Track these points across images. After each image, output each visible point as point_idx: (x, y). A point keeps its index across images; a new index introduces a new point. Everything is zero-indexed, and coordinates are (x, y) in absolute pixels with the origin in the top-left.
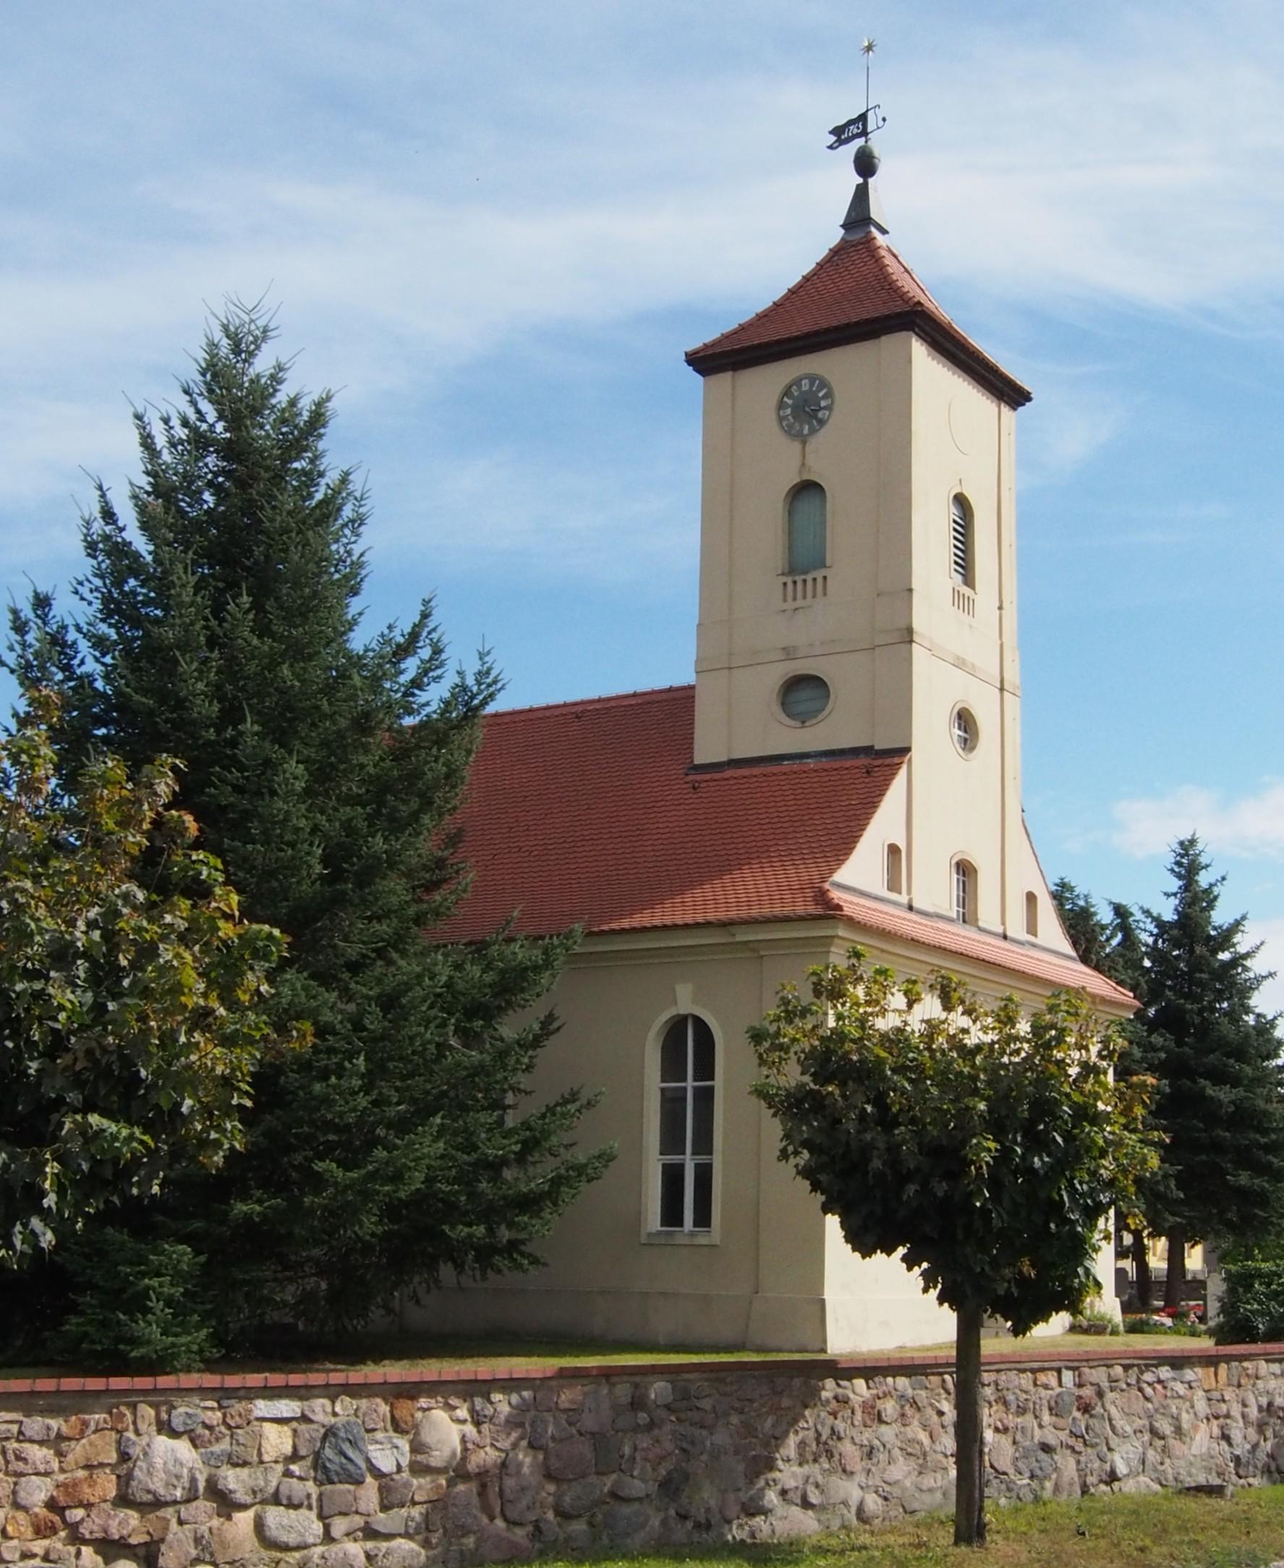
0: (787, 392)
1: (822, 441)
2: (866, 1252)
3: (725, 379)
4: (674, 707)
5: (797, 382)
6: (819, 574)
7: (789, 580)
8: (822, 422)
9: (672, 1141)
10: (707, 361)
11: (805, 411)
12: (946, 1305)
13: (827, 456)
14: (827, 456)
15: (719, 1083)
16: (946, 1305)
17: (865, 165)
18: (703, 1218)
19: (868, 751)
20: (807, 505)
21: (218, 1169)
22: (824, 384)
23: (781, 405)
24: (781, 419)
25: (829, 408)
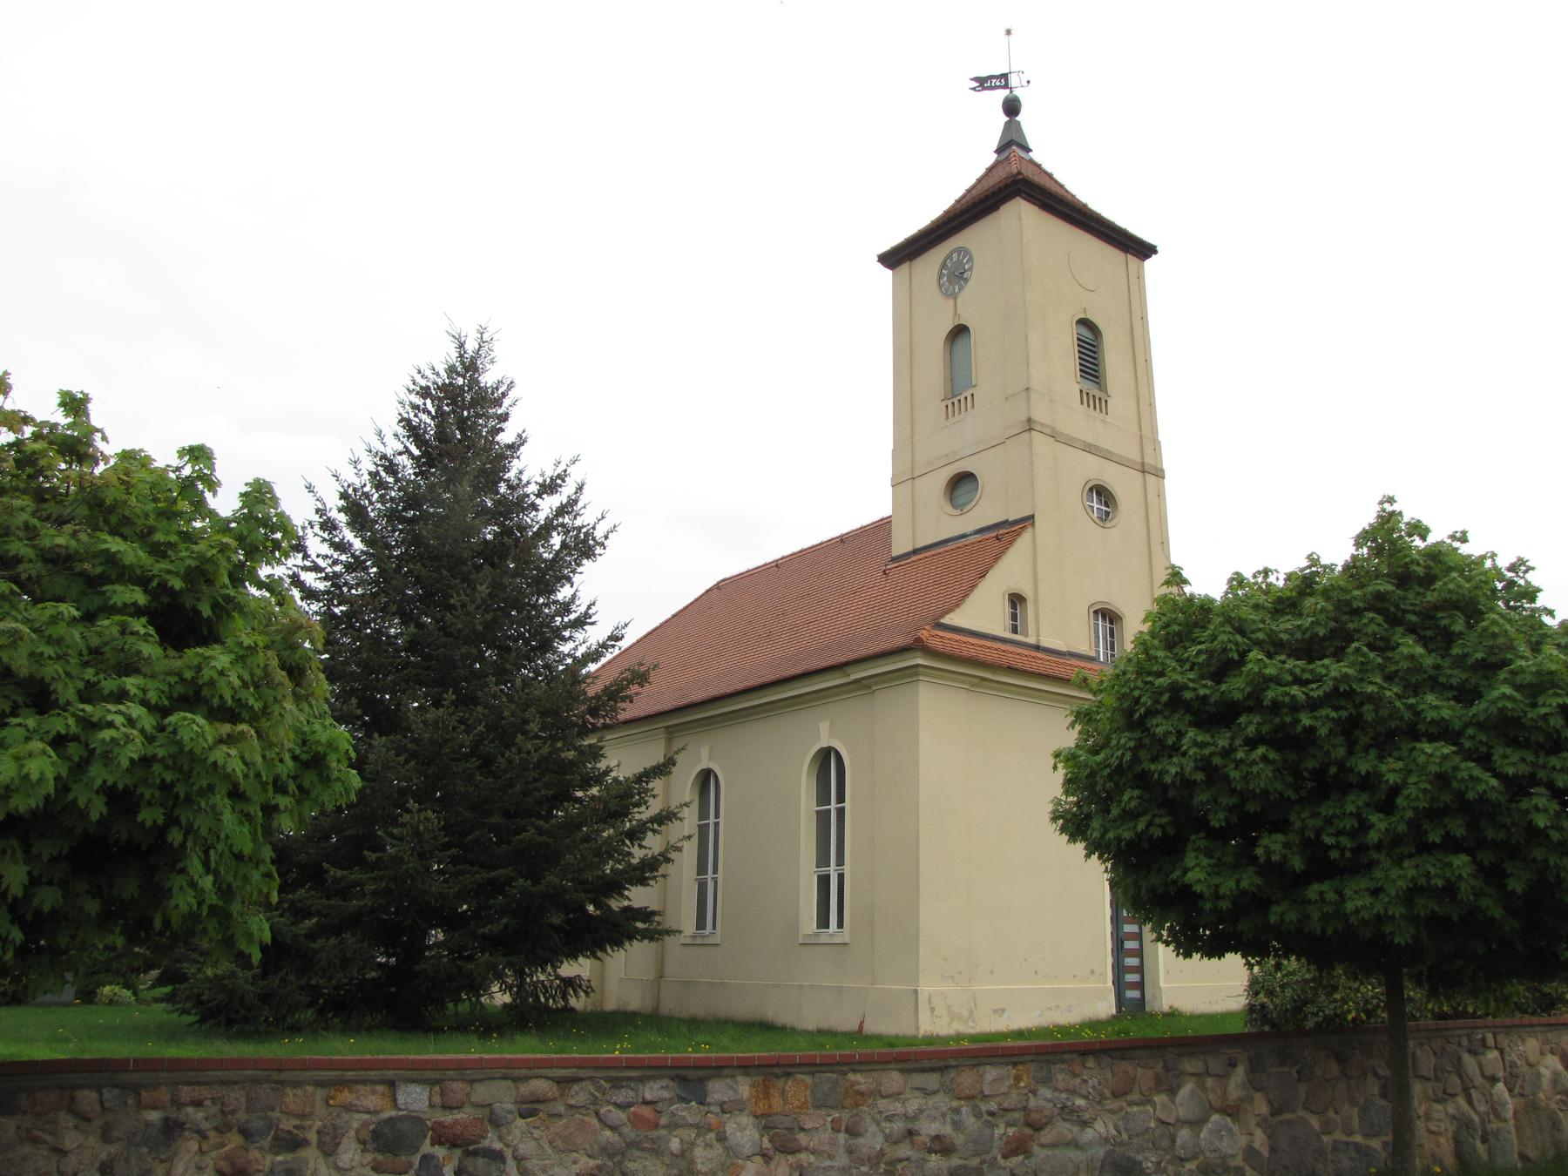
0: (944, 266)
1: (968, 293)
2: (1074, 825)
3: (905, 267)
4: (881, 528)
5: (949, 256)
6: (968, 393)
7: (949, 403)
8: (966, 280)
9: (823, 860)
10: (893, 259)
11: (955, 276)
12: (1095, 857)
13: (972, 306)
14: (972, 306)
15: (847, 805)
16: (1095, 857)
17: (1012, 107)
18: (840, 924)
19: (1004, 524)
20: (960, 344)
21: (500, 976)
22: (967, 252)
23: (940, 276)
24: (940, 286)
25: (971, 269)
